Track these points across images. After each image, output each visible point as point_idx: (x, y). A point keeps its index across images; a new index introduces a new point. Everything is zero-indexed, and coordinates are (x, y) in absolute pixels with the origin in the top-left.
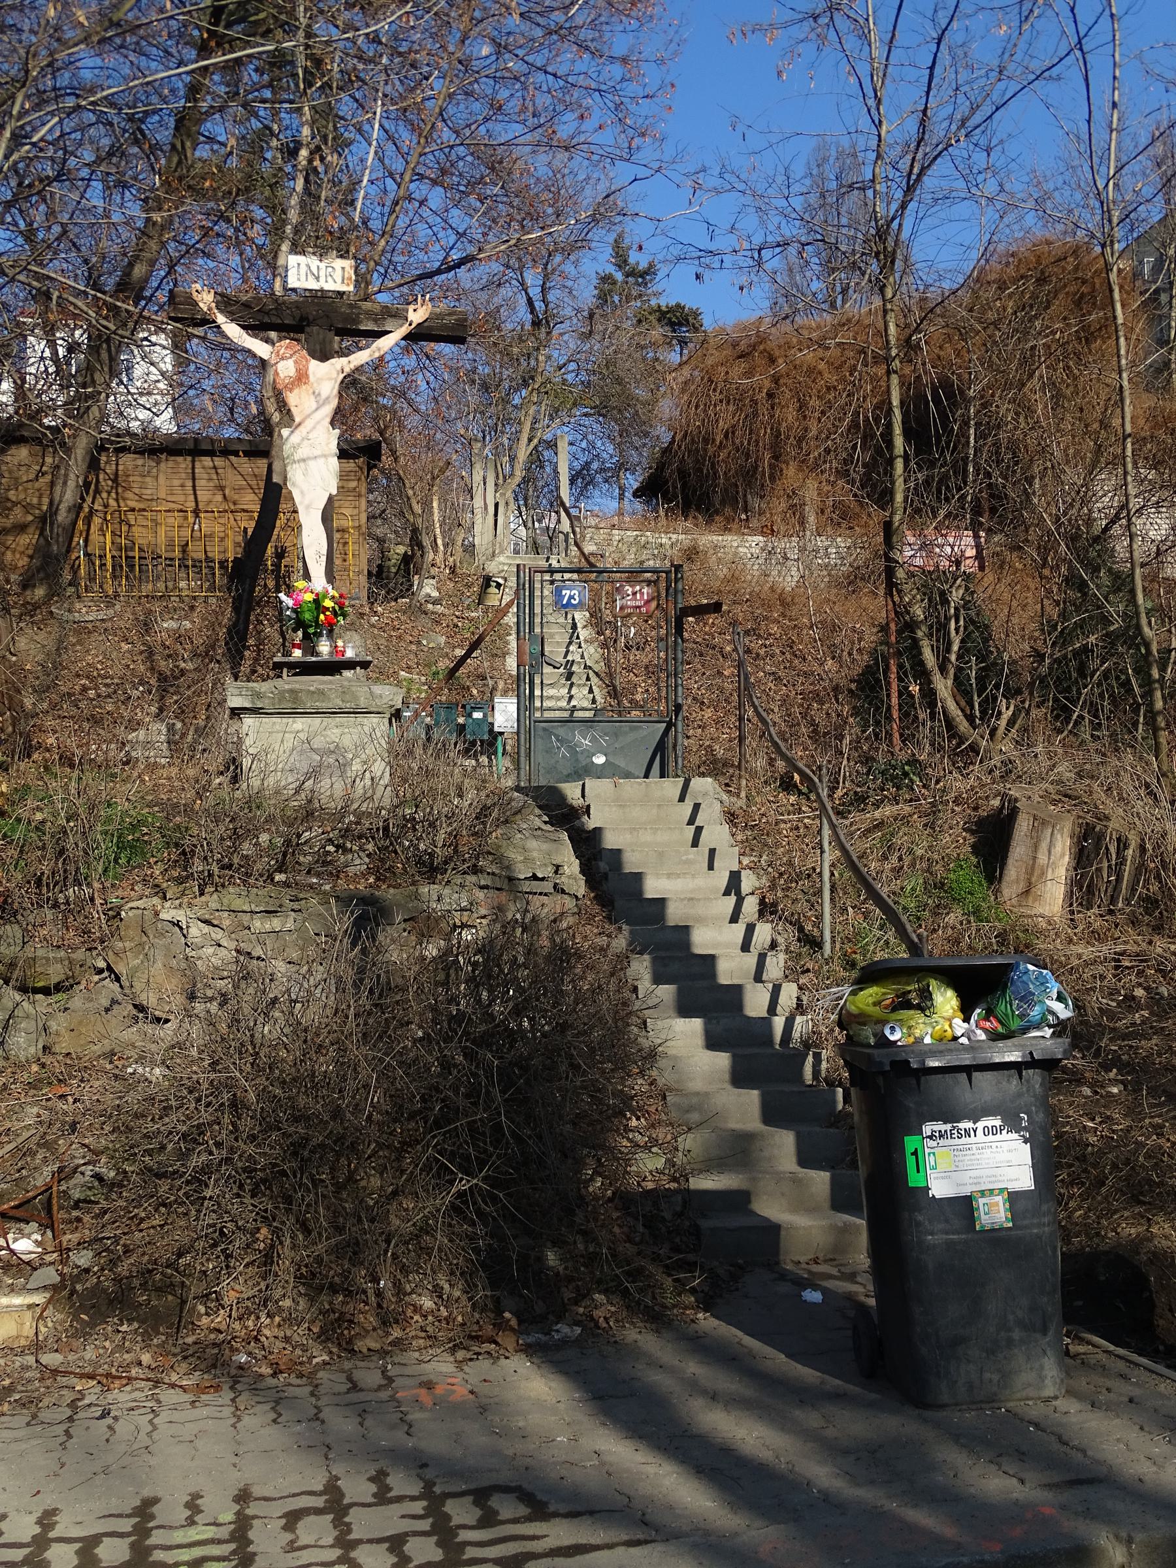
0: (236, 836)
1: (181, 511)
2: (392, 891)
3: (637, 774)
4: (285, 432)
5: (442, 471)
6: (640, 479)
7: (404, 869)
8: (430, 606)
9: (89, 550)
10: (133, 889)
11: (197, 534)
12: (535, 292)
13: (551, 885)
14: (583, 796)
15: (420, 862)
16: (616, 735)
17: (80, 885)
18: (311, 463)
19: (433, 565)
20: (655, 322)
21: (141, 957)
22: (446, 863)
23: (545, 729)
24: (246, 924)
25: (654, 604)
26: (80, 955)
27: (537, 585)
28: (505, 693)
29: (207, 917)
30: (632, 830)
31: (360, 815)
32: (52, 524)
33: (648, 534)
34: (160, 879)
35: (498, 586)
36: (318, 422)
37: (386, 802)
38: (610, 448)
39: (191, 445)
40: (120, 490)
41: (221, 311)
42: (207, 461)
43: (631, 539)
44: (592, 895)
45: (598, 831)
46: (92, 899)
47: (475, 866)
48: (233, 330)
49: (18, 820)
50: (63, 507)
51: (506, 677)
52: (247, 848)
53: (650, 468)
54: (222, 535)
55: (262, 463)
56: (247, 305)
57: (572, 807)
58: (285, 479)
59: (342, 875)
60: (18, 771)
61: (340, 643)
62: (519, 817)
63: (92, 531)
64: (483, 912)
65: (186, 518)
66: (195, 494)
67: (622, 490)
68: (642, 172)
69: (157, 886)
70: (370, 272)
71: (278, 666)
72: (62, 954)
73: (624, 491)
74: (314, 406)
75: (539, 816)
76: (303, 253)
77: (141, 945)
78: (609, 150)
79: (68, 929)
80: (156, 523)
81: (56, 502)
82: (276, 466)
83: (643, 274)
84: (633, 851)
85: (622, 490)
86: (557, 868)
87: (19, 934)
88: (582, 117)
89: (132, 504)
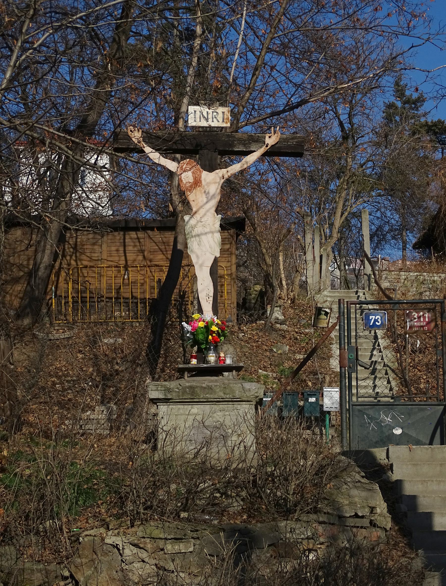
0: (155, 486)
1: (117, 267)
2: (259, 525)
3: (424, 441)
4: (186, 218)
5: (285, 236)
6: (418, 235)
7: (267, 509)
8: (278, 326)
9: (58, 293)
10: (87, 522)
11: (126, 281)
12: (344, 117)
13: (368, 521)
14: (388, 457)
15: (277, 505)
16: (409, 414)
17: (53, 519)
18: (203, 237)
19: (280, 298)
20: (424, 132)
21: (92, 569)
22: (296, 506)
23: (359, 411)
24: (161, 547)
25: (433, 325)
26: (53, 567)
27: (353, 310)
28: (330, 385)
29: (136, 542)
30: (423, 482)
31: (236, 470)
32: (35, 277)
33: (425, 274)
34: (104, 516)
35: (326, 314)
36: (208, 211)
37: (255, 463)
38: (397, 217)
39: (123, 225)
40: (78, 255)
41: (146, 143)
42: (133, 234)
43: (413, 278)
44: (396, 528)
45: (399, 483)
46: (61, 529)
47: (315, 508)
48: (155, 156)
49: (15, 475)
50: (42, 266)
51: (331, 373)
52: (161, 494)
53: (424, 228)
54: (142, 281)
55: (169, 236)
56: (166, 141)
57: (380, 465)
58: (186, 246)
59: (225, 514)
60: (14, 441)
61: (222, 355)
62: (344, 473)
63: (60, 281)
64: (322, 540)
65: (119, 271)
66: (125, 256)
67: (405, 243)
68: (418, 42)
69: (104, 520)
70: (240, 113)
71: (181, 372)
72: (42, 566)
73: (406, 244)
74: (205, 200)
75: (359, 473)
76: (197, 104)
77: (93, 560)
78: (394, 29)
79: (45, 549)
80: (100, 275)
81: (38, 263)
82: (180, 239)
83: (415, 102)
84: (424, 497)
85: (405, 243)
86: (372, 509)
87: (14, 553)
88: (376, 9)
89: (85, 263)
